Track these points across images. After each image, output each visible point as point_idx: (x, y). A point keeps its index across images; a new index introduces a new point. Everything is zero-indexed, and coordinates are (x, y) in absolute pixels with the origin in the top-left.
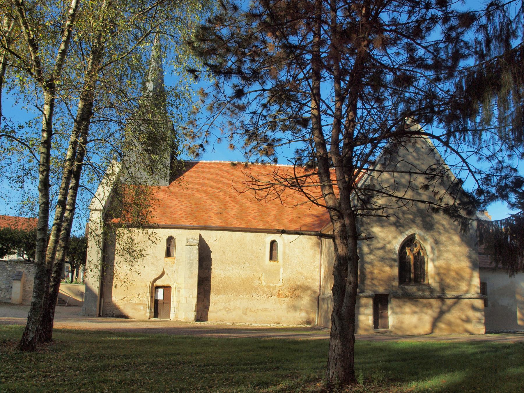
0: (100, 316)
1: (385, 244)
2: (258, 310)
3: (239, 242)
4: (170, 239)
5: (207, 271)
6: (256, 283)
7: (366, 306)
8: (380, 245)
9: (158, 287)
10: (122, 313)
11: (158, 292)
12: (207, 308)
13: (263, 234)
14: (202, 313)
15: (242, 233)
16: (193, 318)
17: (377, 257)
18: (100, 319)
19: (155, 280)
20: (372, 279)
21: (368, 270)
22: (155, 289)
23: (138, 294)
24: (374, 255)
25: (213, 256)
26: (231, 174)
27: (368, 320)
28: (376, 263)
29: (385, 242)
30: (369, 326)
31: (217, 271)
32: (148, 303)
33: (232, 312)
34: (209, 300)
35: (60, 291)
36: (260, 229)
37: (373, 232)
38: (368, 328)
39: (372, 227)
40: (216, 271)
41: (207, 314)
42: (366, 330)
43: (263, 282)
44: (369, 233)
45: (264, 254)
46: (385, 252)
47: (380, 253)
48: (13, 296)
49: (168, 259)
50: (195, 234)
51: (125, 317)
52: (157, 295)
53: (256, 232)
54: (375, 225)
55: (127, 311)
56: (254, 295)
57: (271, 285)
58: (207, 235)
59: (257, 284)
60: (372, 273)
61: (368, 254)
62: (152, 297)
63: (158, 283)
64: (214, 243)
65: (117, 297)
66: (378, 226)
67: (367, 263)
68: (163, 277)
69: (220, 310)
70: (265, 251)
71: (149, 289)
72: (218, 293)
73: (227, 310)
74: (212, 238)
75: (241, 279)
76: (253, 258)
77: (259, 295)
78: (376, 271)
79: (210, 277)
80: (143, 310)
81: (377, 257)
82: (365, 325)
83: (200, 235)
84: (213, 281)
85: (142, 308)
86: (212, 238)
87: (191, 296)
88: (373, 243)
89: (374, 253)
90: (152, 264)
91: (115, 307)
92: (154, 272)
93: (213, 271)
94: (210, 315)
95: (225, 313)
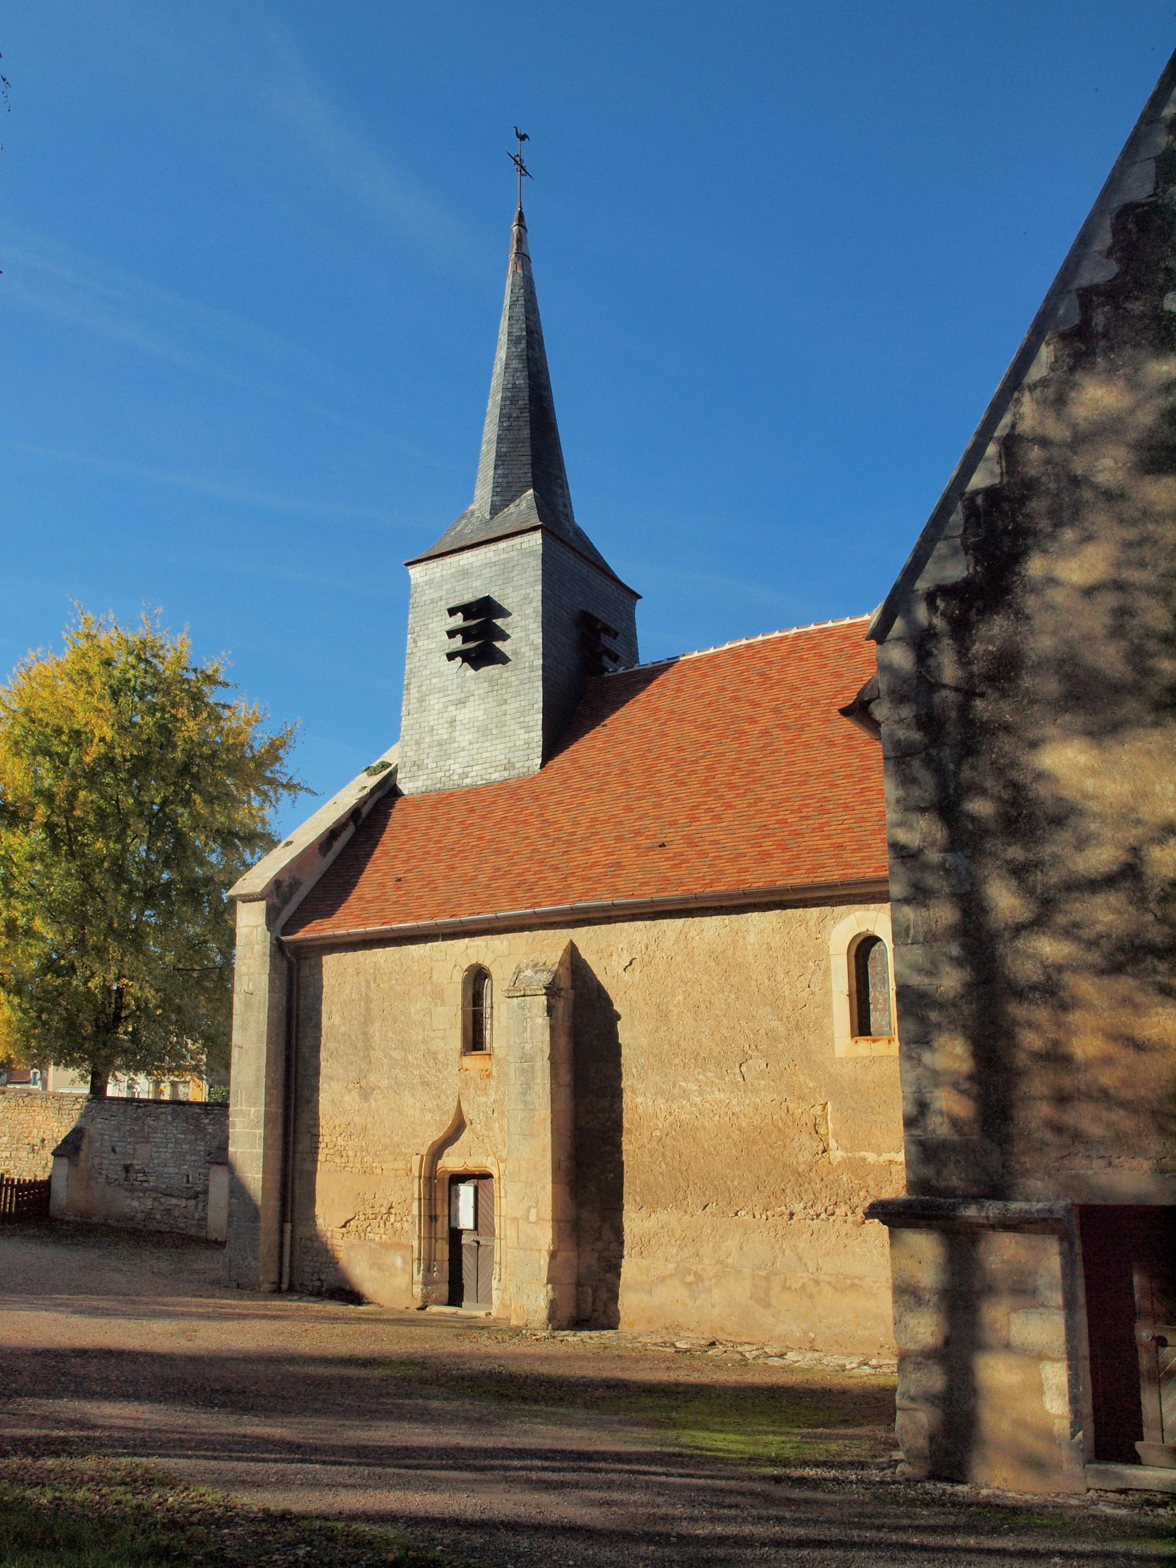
0: (278, 1291)
1: (1135, 850)
2: (817, 1282)
3: (716, 960)
4: (477, 977)
5: (605, 1103)
6: (803, 1149)
7: (1024, 1292)
8: (1101, 857)
9: (458, 1178)
10: (346, 1280)
11: (457, 1196)
12: (612, 1265)
13: (815, 911)
14: (595, 1291)
15: (727, 919)
16: (543, 1314)
17: (1092, 944)
18: (277, 1304)
19: (438, 1151)
20: (1062, 1099)
21: (1031, 1040)
22: (440, 1187)
23: (386, 1205)
24: (1070, 932)
25: (625, 1033)
26: (777, 677)
27: (1040, 1391)
28: (1084, 986)
29: (1133, 835)
30: (1048, 1435)
31: (648, 1102)
32: (416, 1244)
33: (708, 1290)
34: (618, 1231)
35: (903, 1194)
36: (795, 890)
37: (1040, 776)
38: (1040, 1448)
39: (1034, 745)
40: (639, 1100)
41: (615, 1297)
42: (1035, 1464)
43: (833, 1144)
44: (1017, 787)
45: (828, 1008)
46: (1140, 901)
47: (1106, 914)
48: (211, 1215)
49: (474, 1062)
50: (548, 948)
51: (353, 1296)
52: (457, 1210)
53: (782, 905)
54: (1051, 731)
55: (360, 1270)
56: (797, 1207)
57: (871, 1157)
58: (591, 942)
59: (805, 1157)
60: (1056, 1058)
61: (1019, 929)
62: (433, 1218)
63: (452, 1162)
64: (626, 976)
65: (330, 1214)
66: (1069, 734)
67: (1019, 993)
68: (465, 1136)
69: (663, 1279)
70: (828, 993)
71: (415, 1188)
72: (651, 1204)
73: (690, 1279)
74: (611, 952)
75: (736, 1136)
76: (782, 1030)
77: (819, 1208)
78: (1086, 1045)
79: (618, 1127)
80: (404, 1270)
81: (1092, 944)
82: (1019, 1423)
83: (572, 950)
84: (628, 1145)
85: (399, 1262)
86: (611, 952)
87: (533, 1216)
88: (1047, 851)
89: (1061, 920)
90: (423, 1083)
91: (325, 1256)
92: (428, 1116)
93: (627, 1099)
94: (629, 1301)
95: (682, 1293)
